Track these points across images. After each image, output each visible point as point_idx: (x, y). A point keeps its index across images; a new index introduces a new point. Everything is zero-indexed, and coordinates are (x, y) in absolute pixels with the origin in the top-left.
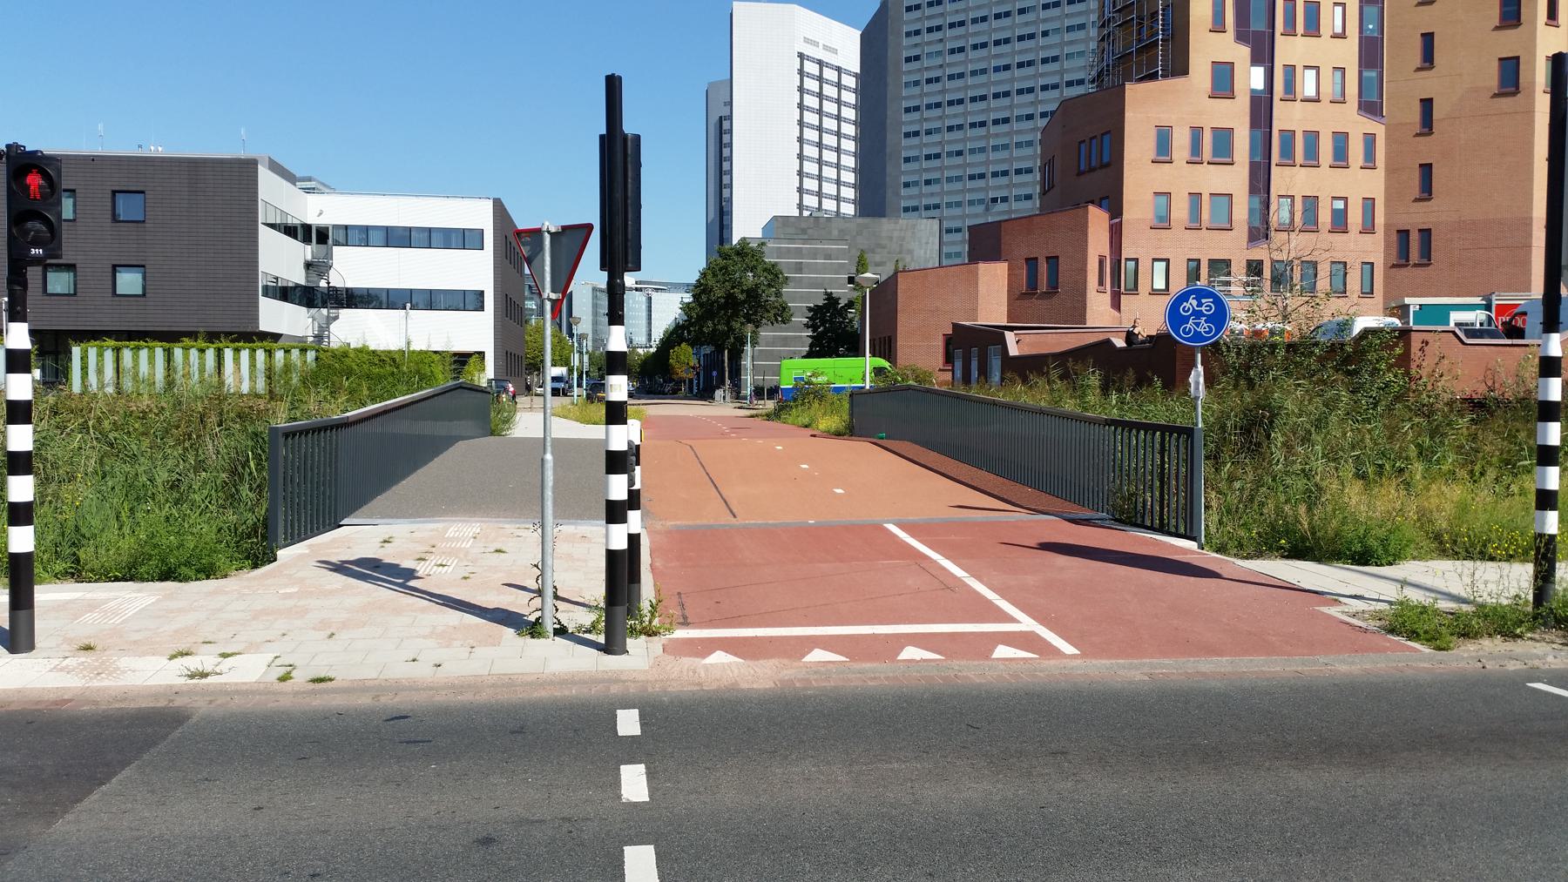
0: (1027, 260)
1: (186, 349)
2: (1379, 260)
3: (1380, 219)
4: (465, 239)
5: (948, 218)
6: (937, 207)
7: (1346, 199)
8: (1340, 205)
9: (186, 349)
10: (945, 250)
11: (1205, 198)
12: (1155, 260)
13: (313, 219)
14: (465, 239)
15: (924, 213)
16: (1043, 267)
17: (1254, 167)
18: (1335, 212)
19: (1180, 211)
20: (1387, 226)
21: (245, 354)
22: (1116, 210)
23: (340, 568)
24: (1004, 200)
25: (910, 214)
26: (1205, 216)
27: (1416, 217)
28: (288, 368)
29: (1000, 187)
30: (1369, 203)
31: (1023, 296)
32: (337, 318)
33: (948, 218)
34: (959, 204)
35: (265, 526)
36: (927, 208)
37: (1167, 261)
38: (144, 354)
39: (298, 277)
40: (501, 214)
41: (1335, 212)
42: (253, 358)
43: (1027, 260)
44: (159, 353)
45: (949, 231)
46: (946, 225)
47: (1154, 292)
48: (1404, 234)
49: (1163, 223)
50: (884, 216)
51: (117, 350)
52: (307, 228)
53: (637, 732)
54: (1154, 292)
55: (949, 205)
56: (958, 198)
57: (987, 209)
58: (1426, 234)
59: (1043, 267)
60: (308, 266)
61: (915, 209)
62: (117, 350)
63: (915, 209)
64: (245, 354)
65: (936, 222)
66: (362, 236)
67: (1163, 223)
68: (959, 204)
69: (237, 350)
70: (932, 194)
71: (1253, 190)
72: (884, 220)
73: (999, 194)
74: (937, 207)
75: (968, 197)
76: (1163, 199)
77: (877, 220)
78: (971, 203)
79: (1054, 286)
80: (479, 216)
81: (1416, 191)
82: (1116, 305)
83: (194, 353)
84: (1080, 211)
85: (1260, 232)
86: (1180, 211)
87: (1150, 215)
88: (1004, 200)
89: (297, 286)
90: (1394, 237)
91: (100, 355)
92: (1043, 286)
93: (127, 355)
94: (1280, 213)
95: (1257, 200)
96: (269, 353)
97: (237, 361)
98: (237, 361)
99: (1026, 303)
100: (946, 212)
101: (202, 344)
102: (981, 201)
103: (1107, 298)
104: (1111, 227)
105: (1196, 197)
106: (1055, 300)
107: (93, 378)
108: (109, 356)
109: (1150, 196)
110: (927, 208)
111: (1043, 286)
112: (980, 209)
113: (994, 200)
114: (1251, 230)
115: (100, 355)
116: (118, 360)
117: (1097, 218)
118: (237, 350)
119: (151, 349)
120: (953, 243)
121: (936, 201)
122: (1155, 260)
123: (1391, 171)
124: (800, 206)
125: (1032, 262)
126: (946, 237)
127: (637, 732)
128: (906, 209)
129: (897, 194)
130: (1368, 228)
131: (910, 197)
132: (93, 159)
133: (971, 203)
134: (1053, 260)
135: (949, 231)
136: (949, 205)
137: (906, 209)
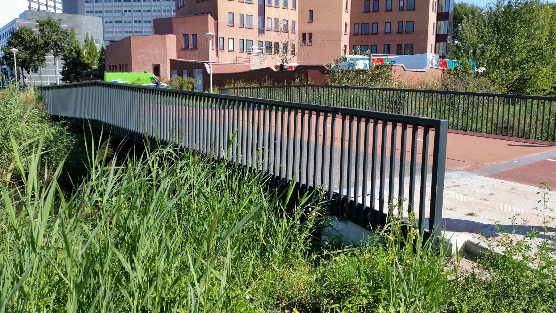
0: (184, 35)
2: (296, 42)
3: (297, 29)
5: (106, 17)
6: (101, 12)
7: (287, 21)
8: (285, 22)
10: (106, 30)
11: (245, 16)
12: (229, 38)
15: (95, 14)
16: (191, 38)
17: (260, 6)
18: (284, 25)
19: (237, 21)
20: (299, 31)
22: (216, 19)
23: (27, 180)
24: (130, 11)
25: (89, 14)
26: (245, 23)
27: (308, 29)
29: (127, 6)
30: (294, 23)
31: (183, 50)
33: (106, 17)
34: (110, 12)
36: (97, 12)
37: (233, 39)
41: (284, 25)
43: (184, 35)
45: (107, 22)
46: (105, 20)
47: (229, 51)
48: (304, 34)
49: (231, 24)
50: (76, 13)
53: (443, 217)
54: (229, 51)
55: (106, 12)
56: (110, 9)
57: (123, 15)
58: (311, 34)
59: (191, 38)
61: (91, 12)
63: (91, 12)
65: (101, 18)
67: (231, 24)
68: (110, 12)
70: (99, 7)
71: (260, 15)
72: (78, 16)
73: (127, 9)
74: (101, 12)
75: (114, 9)
76: (231, 15)
77: (75, 15)
78: (116, 11)
79: (196, 47)
81: (308, 20)
82: (217, 56)
84: (205, 17)
85: (262, 31)
86: (237, 21)
87: (227, 21)
88: (130, 11)
90: (301, 35)
92: (191, 46)
94: (268, 24)
95: (261, 18)
99: (184, 52)
100: (105, 15)
102: (120, 11)
103: (214, 52)
104: (215, 24)
105: (242, 15)
106: (196, 51)
109: (227, 13)
110: (97, 12)
111: (191, 46)
112: (120, 14)
113: (125, 11)
114: (259, 29)
117: (210, 18)
120: (109, 27)
121: (100, 9)
122: (229, 38)
123: (300, 12)
124: (30, 7)
125: (186, 36)
126: (106, 25)
127: (443, 217)
128: (87, 12)
129: (83, 5)
130: (294, 32)
131: (89, 7)
133: (116, 11)
134: (195, 36)
135: (107, 22)
136: (106, 12)
137: (87, 12)
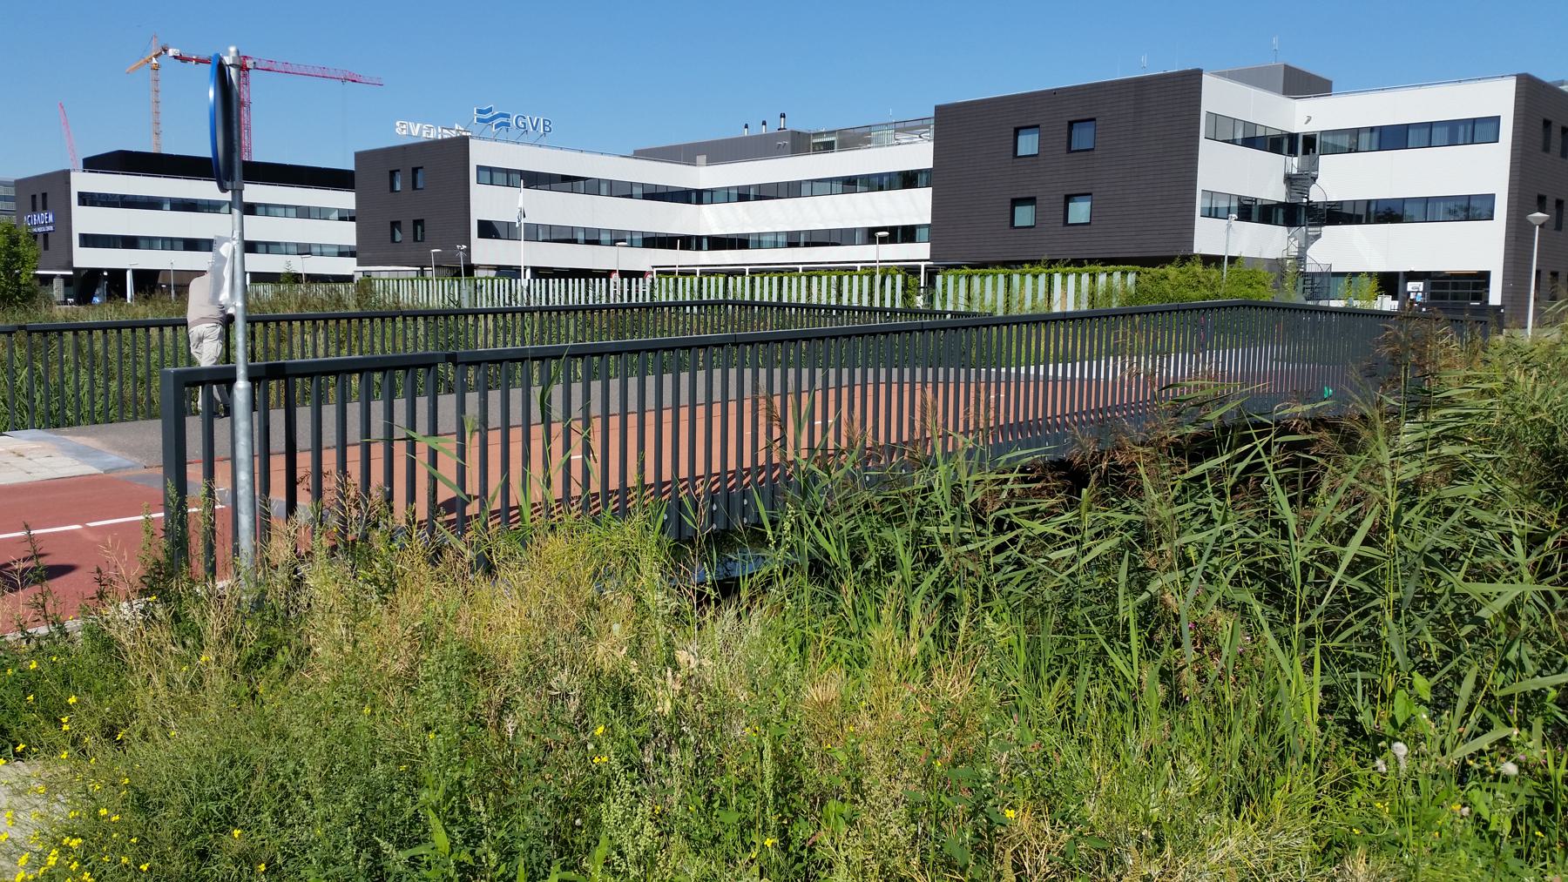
1: (1023, 275)
4: (1475, 131)
9: (1023, 275)
13: (1299, 127)
14: (1475, 131)
21: (1072, 279)
28: (1109, 293)
32: (1318, 237)
35: (1202, 448)
38: (989, 280)
39: (1275, 192)
40: (1531, 92)
42: (1078, 282)
44: (1001, 278)
51: (969, 277)
52: (1293, 137)
60: (1289, 179)
62: (969, 277)
64: (1072, 279)
66: (1352, 141)
69: (1065, 275)
80: (1497, 98)
83: (1029, 278)
89: (1280, 205)
91: (956, 282)
93: (976, 281)
96: (1093, 276)
97: (1064, 285)
98: (1064, 285)
101: (967, 270)
107: (388, 345)
108: (963, 282)
115: (956, 282)
116: (1008, 286)
118: (1065, 275)
119: (995, 275)
132: (1055, 92)
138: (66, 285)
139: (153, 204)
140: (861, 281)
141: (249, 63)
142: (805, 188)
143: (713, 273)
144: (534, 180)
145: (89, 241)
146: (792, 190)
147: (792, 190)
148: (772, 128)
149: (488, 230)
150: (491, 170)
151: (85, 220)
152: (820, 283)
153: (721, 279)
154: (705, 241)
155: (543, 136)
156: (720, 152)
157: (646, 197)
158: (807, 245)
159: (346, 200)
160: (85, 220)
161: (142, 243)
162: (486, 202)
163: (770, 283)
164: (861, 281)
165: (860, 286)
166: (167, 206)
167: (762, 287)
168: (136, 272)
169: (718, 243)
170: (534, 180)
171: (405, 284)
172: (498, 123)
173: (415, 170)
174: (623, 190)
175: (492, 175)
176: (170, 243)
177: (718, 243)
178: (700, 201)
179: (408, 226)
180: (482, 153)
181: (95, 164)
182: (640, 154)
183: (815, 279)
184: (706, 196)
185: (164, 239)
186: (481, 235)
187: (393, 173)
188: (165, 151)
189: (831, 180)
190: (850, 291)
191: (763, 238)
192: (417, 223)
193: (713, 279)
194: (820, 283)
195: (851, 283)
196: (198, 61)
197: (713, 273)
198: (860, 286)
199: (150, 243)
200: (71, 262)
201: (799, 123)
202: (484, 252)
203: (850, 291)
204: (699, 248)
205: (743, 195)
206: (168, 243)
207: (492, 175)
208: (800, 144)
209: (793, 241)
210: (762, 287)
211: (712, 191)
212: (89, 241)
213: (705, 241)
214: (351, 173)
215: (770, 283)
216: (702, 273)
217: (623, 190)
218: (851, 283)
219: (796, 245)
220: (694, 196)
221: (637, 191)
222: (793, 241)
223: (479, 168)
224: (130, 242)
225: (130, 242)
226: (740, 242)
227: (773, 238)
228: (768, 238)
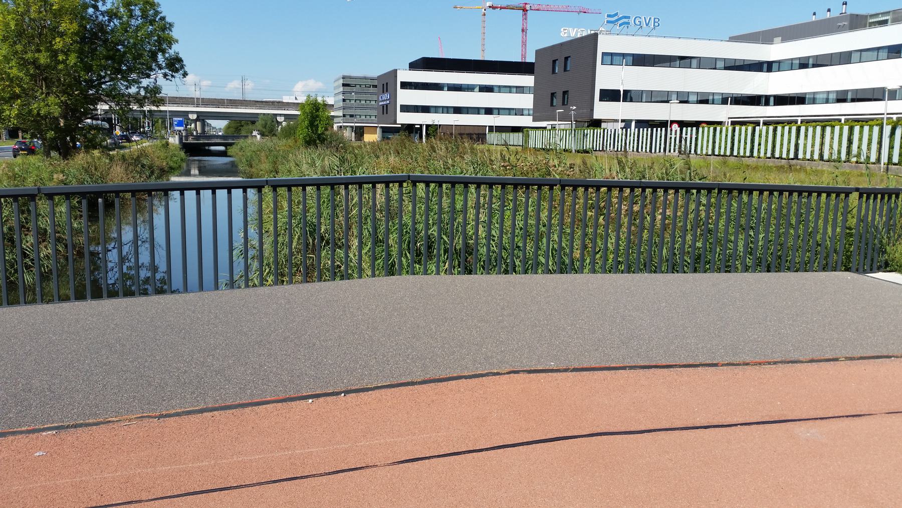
138: (383, 132)
139: (469, 88)
140: (871, 130)
141: (528, 7)
142: (855, 57)
143: (742, 123)
144: (641, 60)
145: (406, 109)
146: (844, 58)
147: (844, 58)
148: (835, 13)
149: (610, 95)
150: (612, 54)
151: (405, 97)
152: (833, 132)
153: (750, 128)
154: (772, 99)
155: (654, 27)
156: (790, 33)
157: (726, 68)
158: (853, 100)
159: (528, 80)
160: (405, 97)
161: (432, 109)
162: (607, 77)
163: (790, 132)
164: (871, 130)
165: (870, 136)
166: (446, 88)
167: (782, 135)
168: (428, 126)
169: (781, 100)
170: (641, 60)
171: (560, 133)
172: (619, 22)
173: (566, 59)
174: (711, 64)
175: (612, 58)
176: (446, 110)
177: (781, 100)
178: (769, 70)
179: (559, 95)
180: (605, 45)
181: (414, 66)
182: (734, 39)
183: (828, 129)
184: (775, 66)
185: (443, 107)
186: (601, 100)
187: (554, 62)
188: (486, 59)
189: (878, 49)
190: (860, 139)
191: (818, 96)
192: (565, 93)
193: (744, 128)
194: (833, 132)
195: (861, 132)
196: (501, 8)
197: (742, 123)
198: (870, 136)
199: (500, 111)
200: (395, 121)
201: (855, 8)
202: (602, 110)
203: (860, 139)
204: (767, 104)
205: (804, 64)
206: (445, 110)
207: (612, 58)
208: (857, 22)
209: (842, 98)
210: (782, 135)
211: (779, 62)
212: (406, 109)
213: (772, 99)
214: (532, 64)
215: (790, 132)
216: (847, 121)
217: (711, 64)
218: (861, 132)
219: (844, 100)
220: (765, 66)
221: (720, 64)
222: (842, 98)
223: (604, 54)
224: (426, 109)
225: (426, 109)
226: (799, 100)
227: (825, 96)
228: (821, 96)
